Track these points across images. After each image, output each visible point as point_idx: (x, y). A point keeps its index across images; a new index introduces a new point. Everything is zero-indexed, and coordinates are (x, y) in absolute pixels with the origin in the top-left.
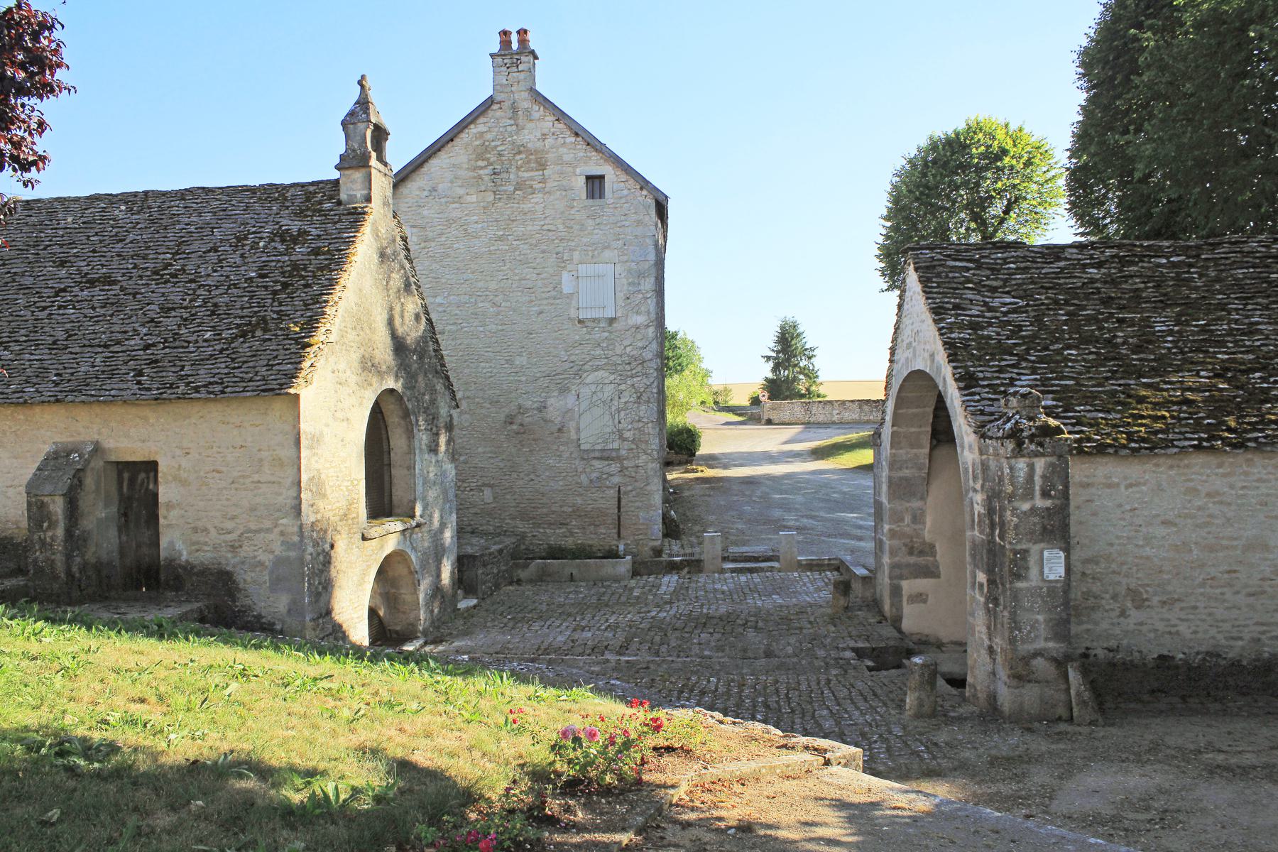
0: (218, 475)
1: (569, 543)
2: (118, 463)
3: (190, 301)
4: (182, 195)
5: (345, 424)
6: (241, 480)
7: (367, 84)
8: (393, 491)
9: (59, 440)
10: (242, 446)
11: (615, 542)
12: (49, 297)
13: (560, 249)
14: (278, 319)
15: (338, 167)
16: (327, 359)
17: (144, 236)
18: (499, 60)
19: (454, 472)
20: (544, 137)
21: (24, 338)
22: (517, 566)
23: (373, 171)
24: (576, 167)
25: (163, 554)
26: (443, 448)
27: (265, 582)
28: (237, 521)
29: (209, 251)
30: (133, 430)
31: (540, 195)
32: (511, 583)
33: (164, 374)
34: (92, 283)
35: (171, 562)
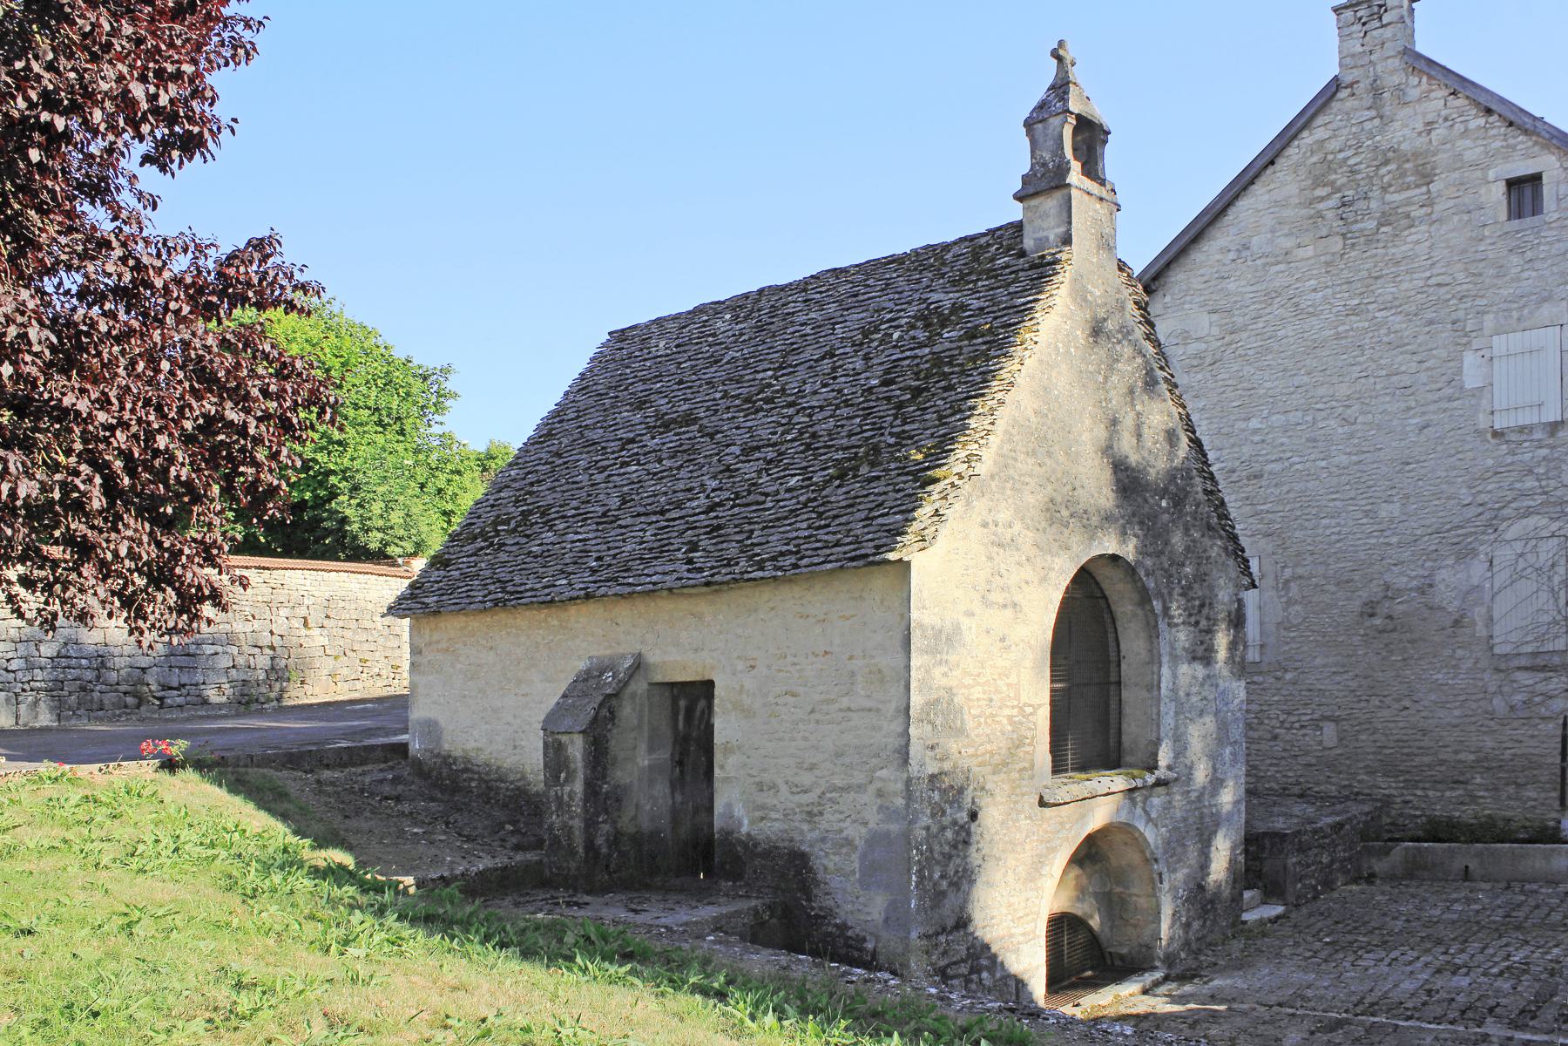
0: (792, 700)
1: (1467, 814)
2: (672, 685)
3: (782, 434)
4: (803, 286)
5: (1009, 612)
6: (825, 707)
7: (1069, 54)
8: (1124, 726)
9: (595, 653)
10: (826, 653)
11: (1554, 815)
12: (613, 453)
13: (1461, 314)
14: (896, 444)
15: (1019, 197)
16: (968, 504)
17: (745, 351)
18: (1349, 14)
19: (1243, 695)
20: (1429, 126)
21: (573, 512)
22: (1369, 852)
23: (1074, 192)
24: (1488, 167)
25: (718, 823)
26: (1222, 654)
27: (853, 872)
28: (817, 772)
29: (823, 358)
30: (684, 635)
31: (1424, 228)
32: (1356, 881)
33: (725, 545)
34: (667, 426)
35: (727, 833)
